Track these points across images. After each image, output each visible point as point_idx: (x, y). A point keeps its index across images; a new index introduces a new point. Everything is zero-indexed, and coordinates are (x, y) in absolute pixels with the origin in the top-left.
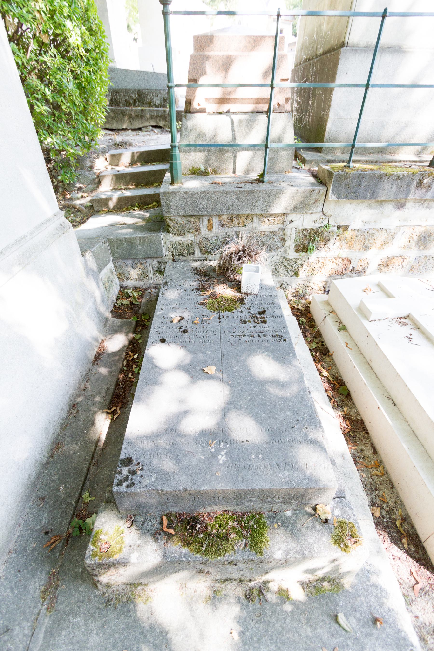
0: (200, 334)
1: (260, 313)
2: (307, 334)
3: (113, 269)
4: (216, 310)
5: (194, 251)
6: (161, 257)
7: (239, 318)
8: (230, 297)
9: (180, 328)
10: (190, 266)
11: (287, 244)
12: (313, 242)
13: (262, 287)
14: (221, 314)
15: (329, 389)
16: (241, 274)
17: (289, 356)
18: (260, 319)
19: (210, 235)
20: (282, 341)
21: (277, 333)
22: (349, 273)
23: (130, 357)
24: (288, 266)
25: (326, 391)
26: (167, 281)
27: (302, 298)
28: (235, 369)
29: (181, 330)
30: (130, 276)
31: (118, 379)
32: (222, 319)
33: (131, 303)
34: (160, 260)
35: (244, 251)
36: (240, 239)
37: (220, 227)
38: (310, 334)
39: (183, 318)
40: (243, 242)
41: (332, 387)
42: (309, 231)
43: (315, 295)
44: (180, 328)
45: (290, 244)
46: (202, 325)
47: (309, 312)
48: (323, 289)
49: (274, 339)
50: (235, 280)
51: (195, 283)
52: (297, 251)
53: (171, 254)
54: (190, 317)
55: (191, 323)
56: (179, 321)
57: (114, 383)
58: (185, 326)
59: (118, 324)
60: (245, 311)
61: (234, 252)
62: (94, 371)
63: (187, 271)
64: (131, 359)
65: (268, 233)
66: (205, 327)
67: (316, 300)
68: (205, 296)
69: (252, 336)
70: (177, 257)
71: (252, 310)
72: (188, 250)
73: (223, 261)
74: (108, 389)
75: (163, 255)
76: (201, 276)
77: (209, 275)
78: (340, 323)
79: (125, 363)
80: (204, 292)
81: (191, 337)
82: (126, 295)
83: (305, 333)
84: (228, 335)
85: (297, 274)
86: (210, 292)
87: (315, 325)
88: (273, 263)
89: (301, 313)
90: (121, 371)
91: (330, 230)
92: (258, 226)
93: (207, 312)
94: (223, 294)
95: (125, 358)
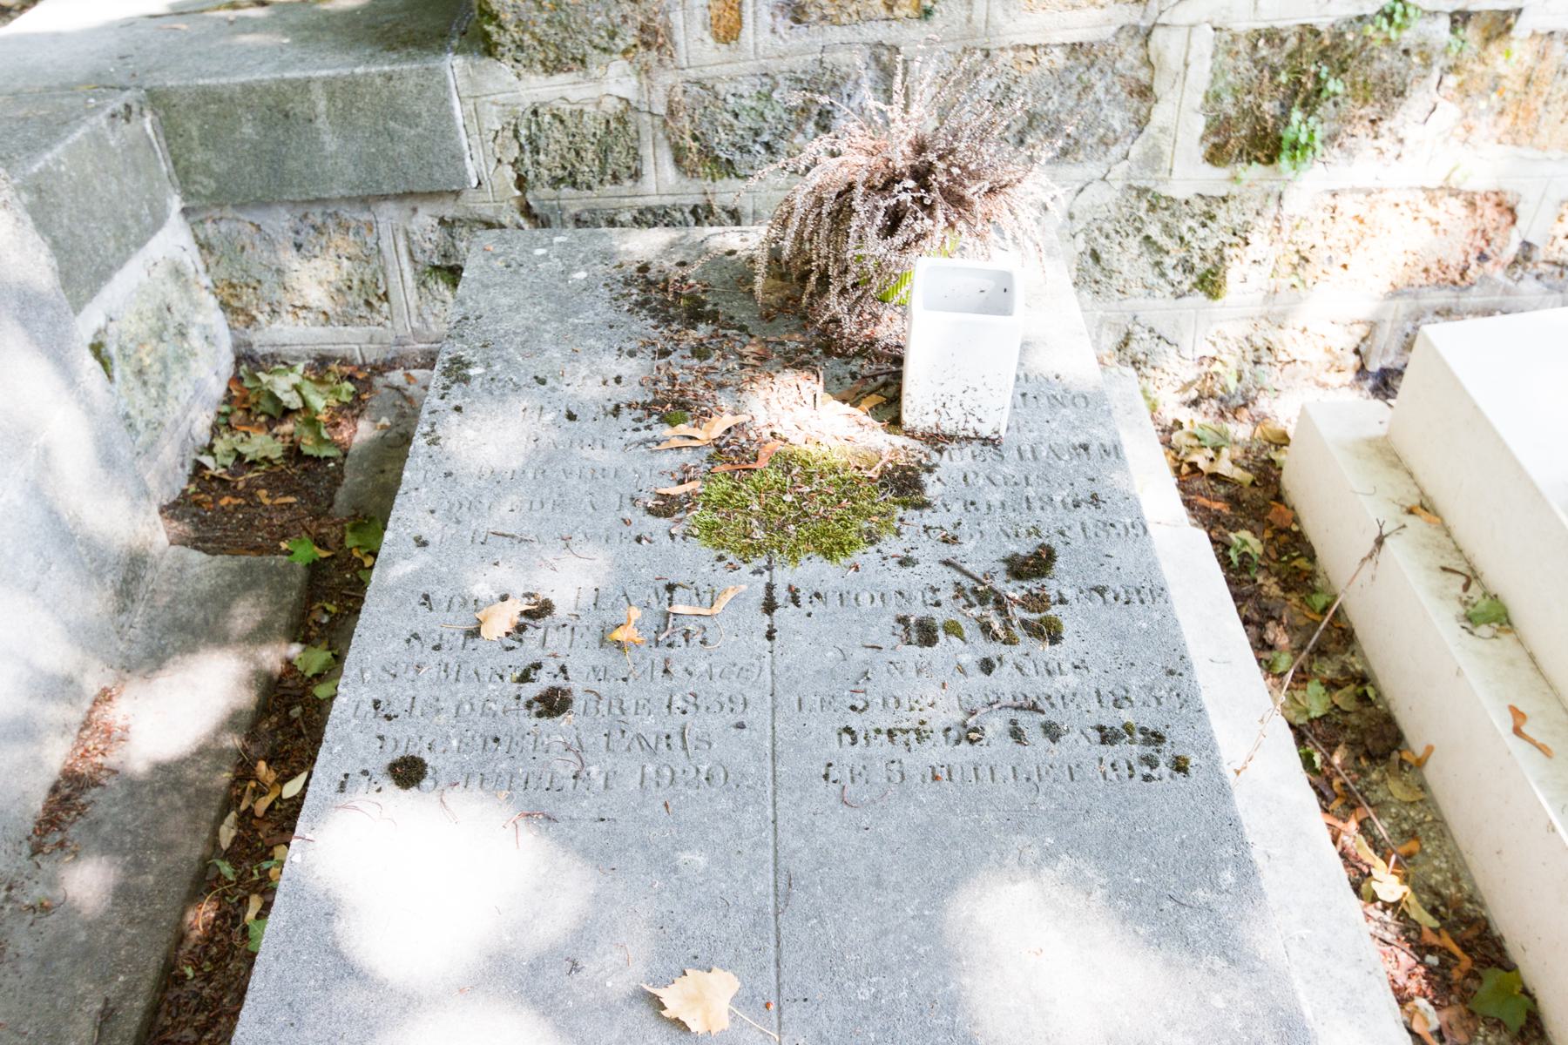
0: (648, 724)
1: (1019, 568)
2: (1274, 633)
3: (191, 259)
4: (750, 550)
5: (637, 157)
6: (457, 194)
7: (894, 609)
8: (838, 459)
9: (525, 678)
10: (607, 256)
11: (1161, 114)
12: (1309, 106)
13: (1033, 392)
14: (784, 576)
15: (1412, 986)
16: (904, 309)
17: (1214, 886)
18: (1018, 613)
19: (726, 69)
20: (1164, 769)
21: (1126, 715)
22: (1499, 274)
23: (260, 792)
24: (1163, 240)
25: (1403, 999)
26: (467, 355)
27: (1235, 412)
28: (865, 994)
29: (531, 690)
30: (286, 299)
31: (181, 938)
32: (786, 615)
33: (294, 453)
34: (449, 212)
35: (922, 175)
36: (898, 98)
37: (783, 23)
38: (1291, 629)
39: (545, 609)
40: (912, 120)
41: (1430, 970)
42: (1292, 42)
43: (1312, 395)
44: (525, 678)
45: (1182, 118)
46: (658, 655)
47: (1279, 498)
48: (1354, 360)
49: (1110, 753)
50: (868, 349)
51: (629, 368)
52: (1216, 155)
53: (510, 174)
54: (588, 599)
55: (592, 639)
56: (521, 628)
57: (152, 973)
58: (551, 666)
59: (205, 585)
60: (929, 552)
61: (860, 178)
62: (37, 893)
63: (588, 287)
64: (262, 805)
65: (1059, 58)
66: (676, 669)
67: (1316, 411)
68: (686, 457)
69: (970, 735)
70: (546, 192)
71: (968, 545)
72: (604, 152)
73: (799, 234)
74: (107, 1015)
75: (465, 182)
76: (667, 321)
77: (713, 317)
78: (1471, 578)
79: (227, 833)
80: (683, 428)
81: (588, 741)
82: (267, 406)
83: (1261, 626)
84: (824, 726)
85: (1210, 283)
86: (716, 428)
87: (1312, 575)
88: (1079, 225)
89: (1234, 500)
90: (203, 883)
91: (1408, 37)
92: (999, 16)
93: (693, 559)
94: (797, 439)
95: (229, 803)
